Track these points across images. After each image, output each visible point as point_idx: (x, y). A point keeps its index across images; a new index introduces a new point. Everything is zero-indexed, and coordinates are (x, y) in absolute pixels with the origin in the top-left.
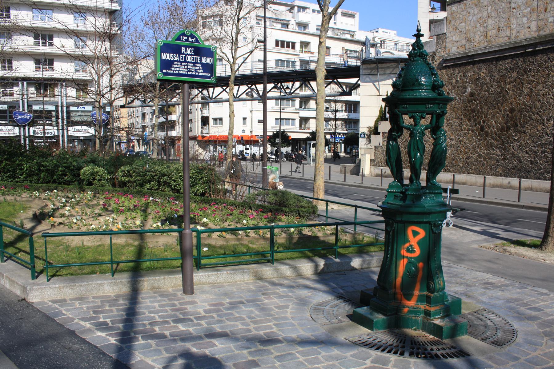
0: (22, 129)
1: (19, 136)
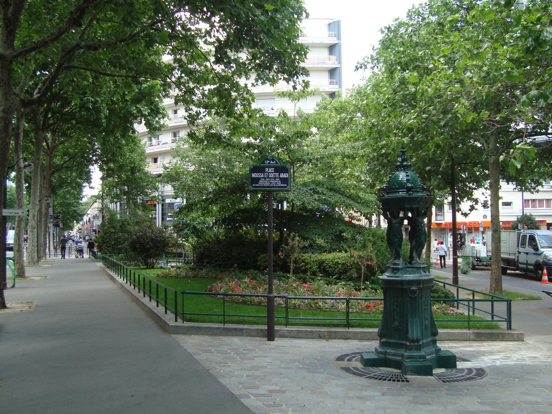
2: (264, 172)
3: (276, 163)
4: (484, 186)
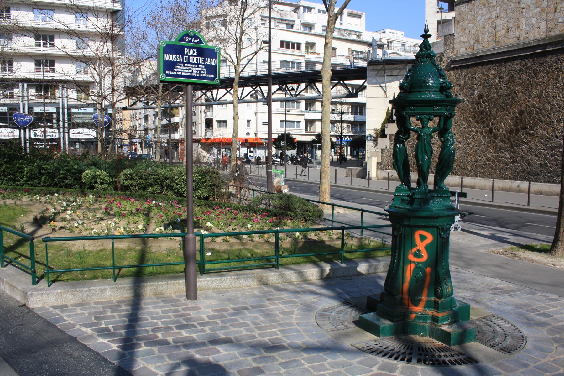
0: (22, 131)
1: (20, 138)
2: (182, 53)
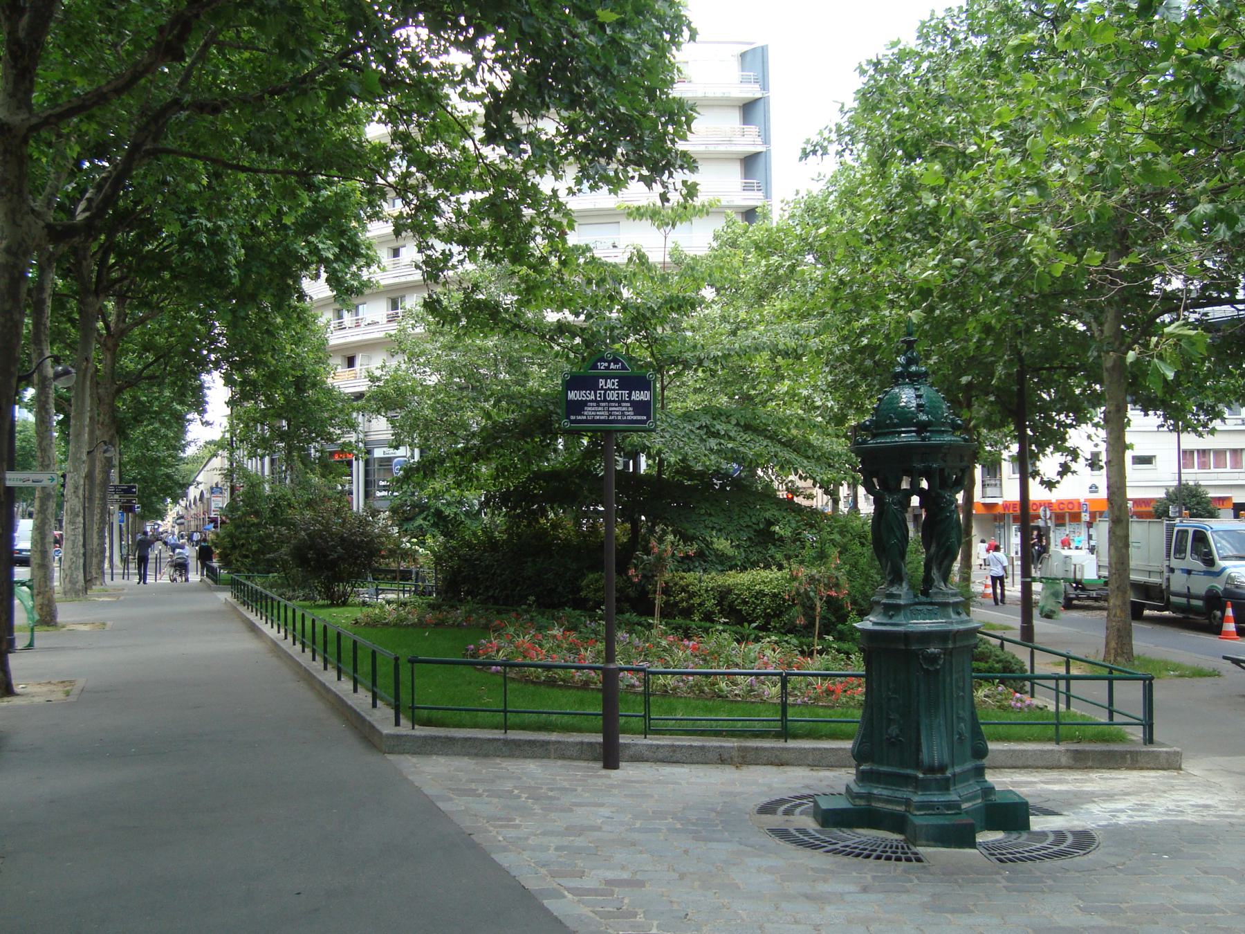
3: (624, 368)
4: (1091, 419)
